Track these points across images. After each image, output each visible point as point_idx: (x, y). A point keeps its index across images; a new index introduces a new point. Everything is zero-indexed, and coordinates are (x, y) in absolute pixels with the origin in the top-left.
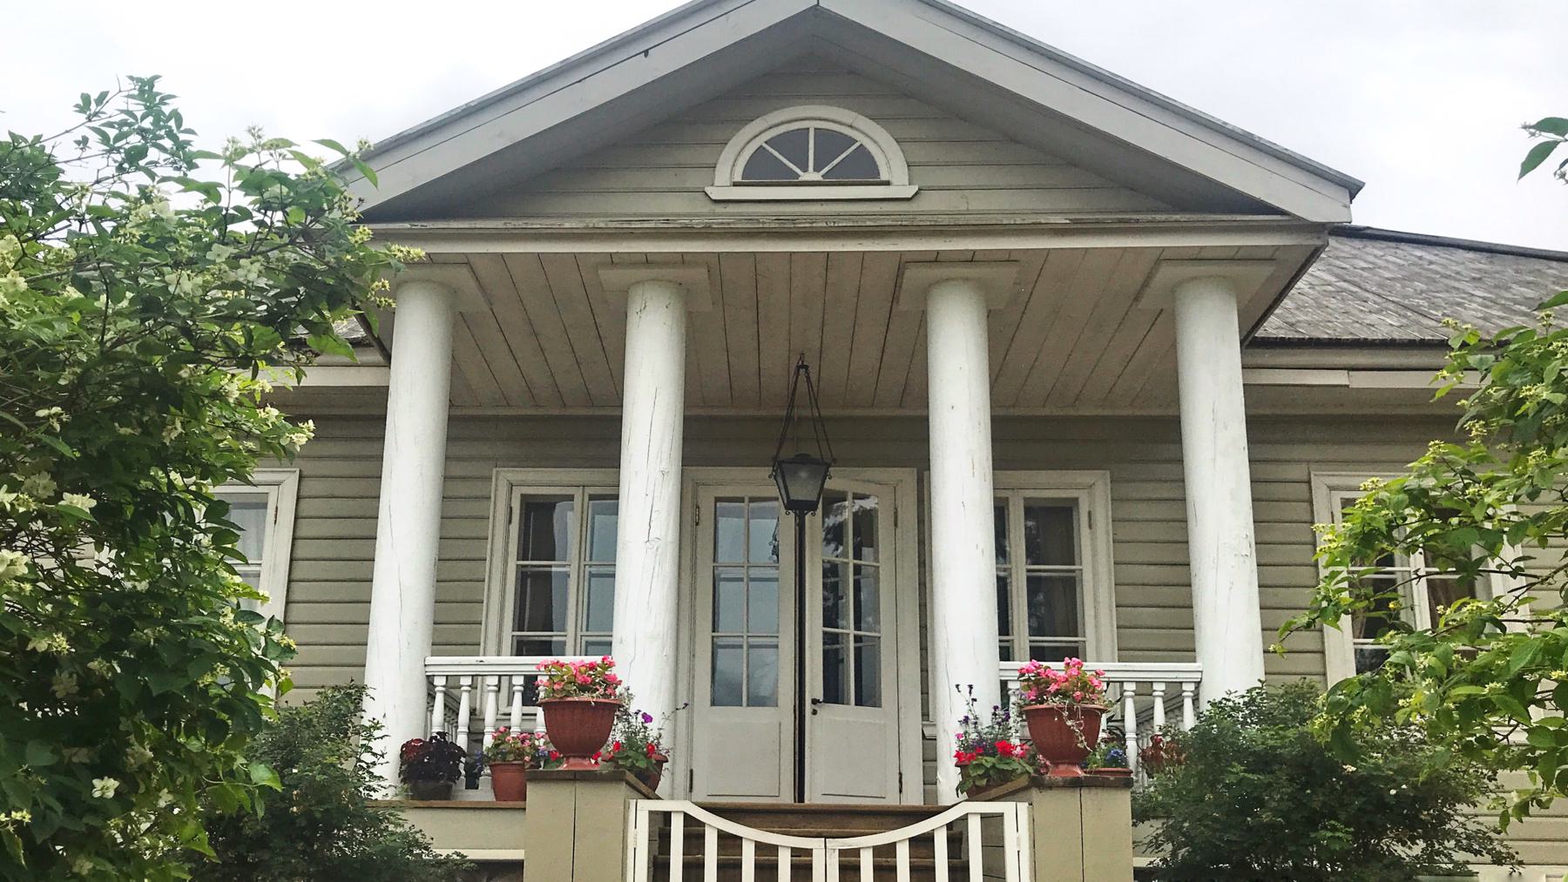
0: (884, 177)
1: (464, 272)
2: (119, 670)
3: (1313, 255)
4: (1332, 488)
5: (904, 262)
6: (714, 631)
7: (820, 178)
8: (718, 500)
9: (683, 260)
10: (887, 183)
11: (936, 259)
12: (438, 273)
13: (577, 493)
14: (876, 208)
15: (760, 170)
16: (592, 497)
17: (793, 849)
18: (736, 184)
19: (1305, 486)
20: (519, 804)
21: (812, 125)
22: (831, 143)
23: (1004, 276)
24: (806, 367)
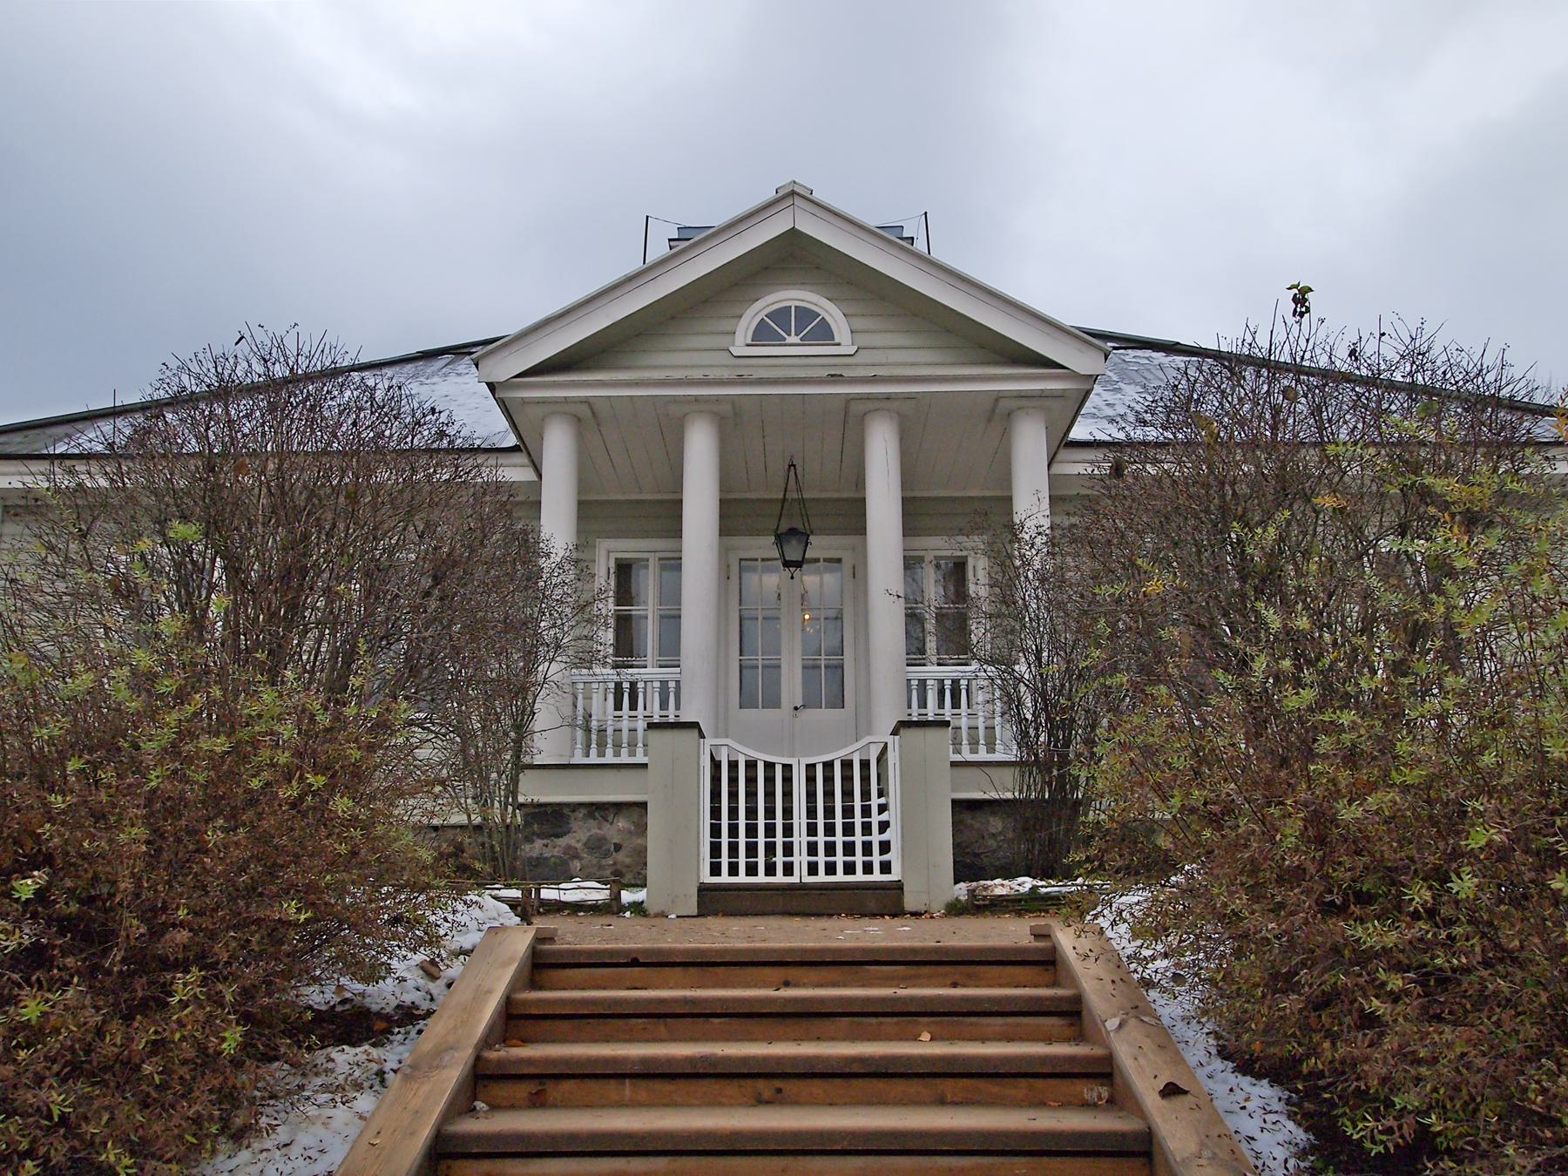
1: (586, 405)
2: (1047, 796)
3: (1088, 393)
5: (850, 399)
6: (741, 655)
7: (799, 342)
8: (741, 560)
9: (718, 399)
10: (839, 344)
11: (868, 397)
13: (651, 557)
15: (762, 334)
17: (897, 912)
18: (748, 345)
20: (908, 554)
21: (793, 304)
22: (805, 315)
23: (726, 408)
24: (794, 466)
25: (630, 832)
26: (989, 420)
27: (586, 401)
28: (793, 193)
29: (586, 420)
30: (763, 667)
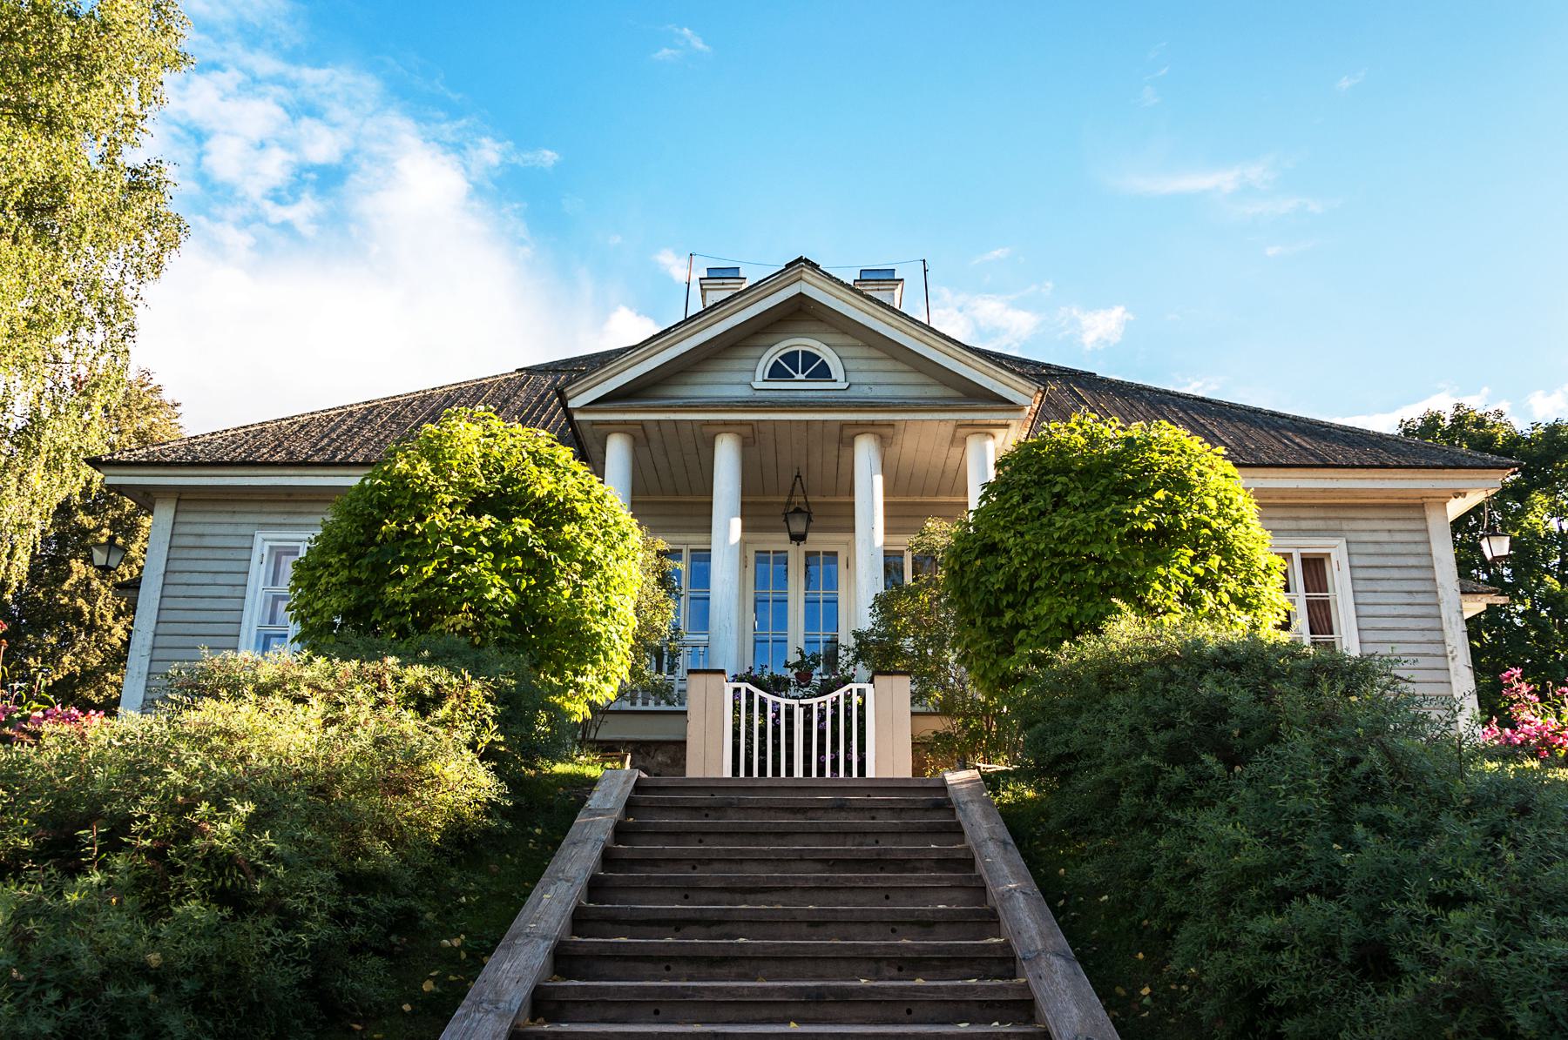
0: (834, 378)
4: (265, 540)
5: (844, 425)
10: (835, 381)
11: (857, 424)
12: (738, 429)
14: (772, 393)
15: (777, 372)
16: (692, 550)
18: (764, 381)
19: (1352, 551)
22: (810, 358)
23: (747, 430)
25: (667, 765)
26: (952, 442)
27: (641, 423)
28: (801, 312)
29: (639, 437)
30: (774, 601)
